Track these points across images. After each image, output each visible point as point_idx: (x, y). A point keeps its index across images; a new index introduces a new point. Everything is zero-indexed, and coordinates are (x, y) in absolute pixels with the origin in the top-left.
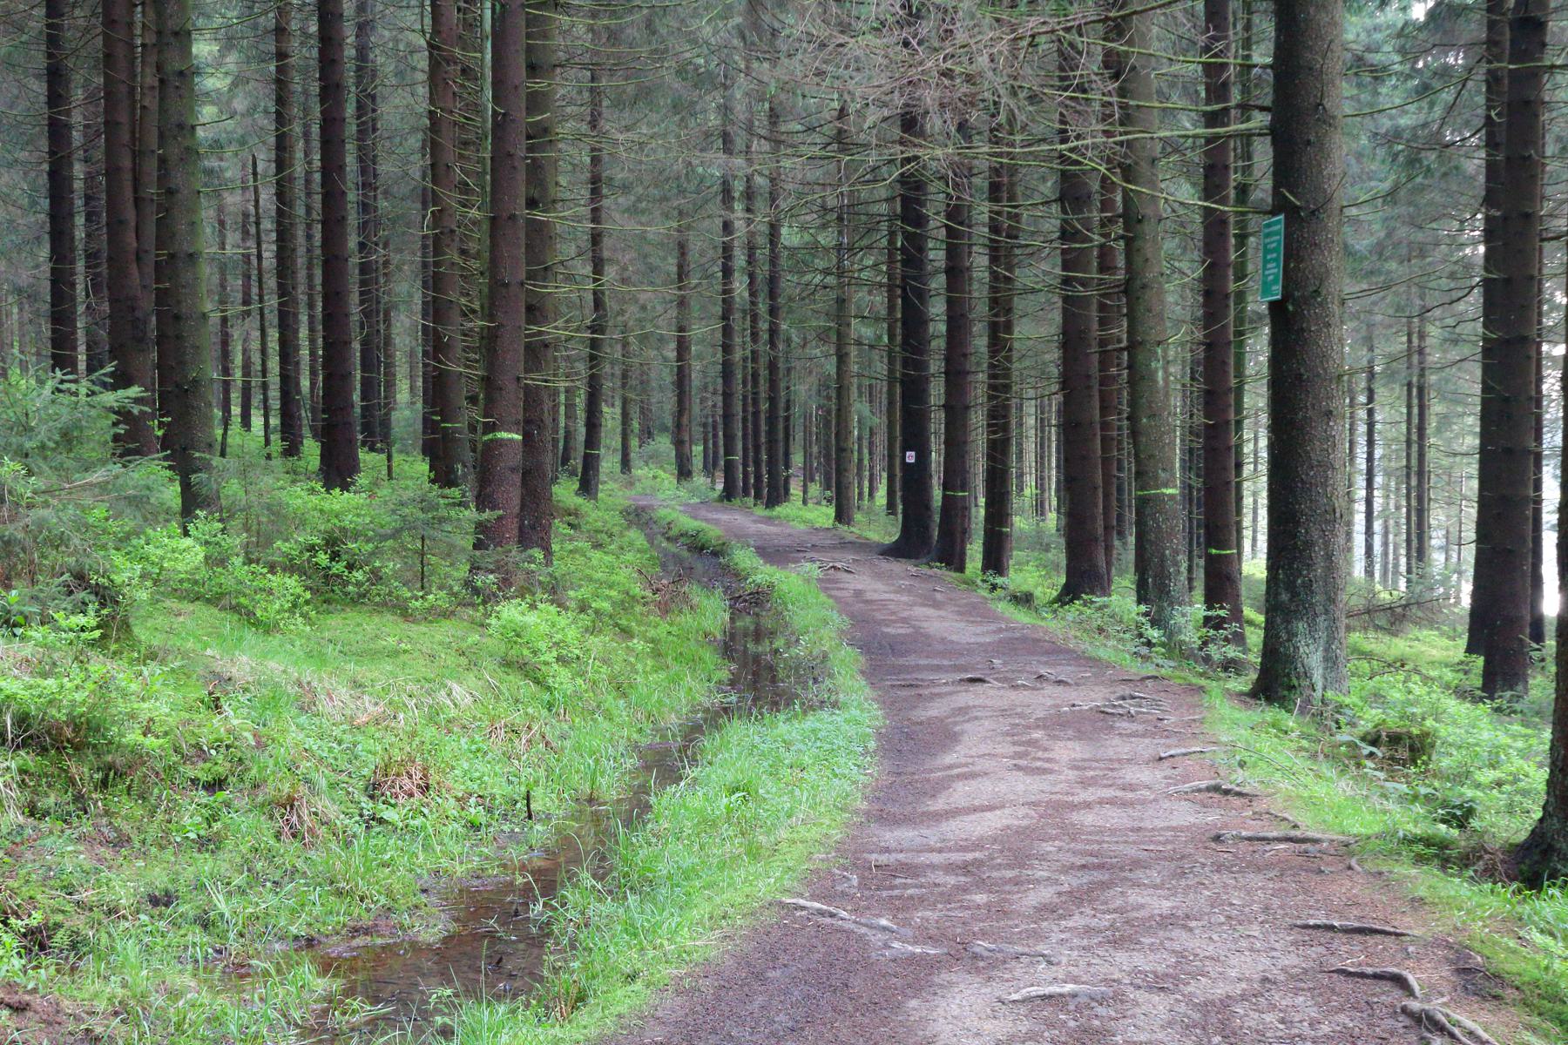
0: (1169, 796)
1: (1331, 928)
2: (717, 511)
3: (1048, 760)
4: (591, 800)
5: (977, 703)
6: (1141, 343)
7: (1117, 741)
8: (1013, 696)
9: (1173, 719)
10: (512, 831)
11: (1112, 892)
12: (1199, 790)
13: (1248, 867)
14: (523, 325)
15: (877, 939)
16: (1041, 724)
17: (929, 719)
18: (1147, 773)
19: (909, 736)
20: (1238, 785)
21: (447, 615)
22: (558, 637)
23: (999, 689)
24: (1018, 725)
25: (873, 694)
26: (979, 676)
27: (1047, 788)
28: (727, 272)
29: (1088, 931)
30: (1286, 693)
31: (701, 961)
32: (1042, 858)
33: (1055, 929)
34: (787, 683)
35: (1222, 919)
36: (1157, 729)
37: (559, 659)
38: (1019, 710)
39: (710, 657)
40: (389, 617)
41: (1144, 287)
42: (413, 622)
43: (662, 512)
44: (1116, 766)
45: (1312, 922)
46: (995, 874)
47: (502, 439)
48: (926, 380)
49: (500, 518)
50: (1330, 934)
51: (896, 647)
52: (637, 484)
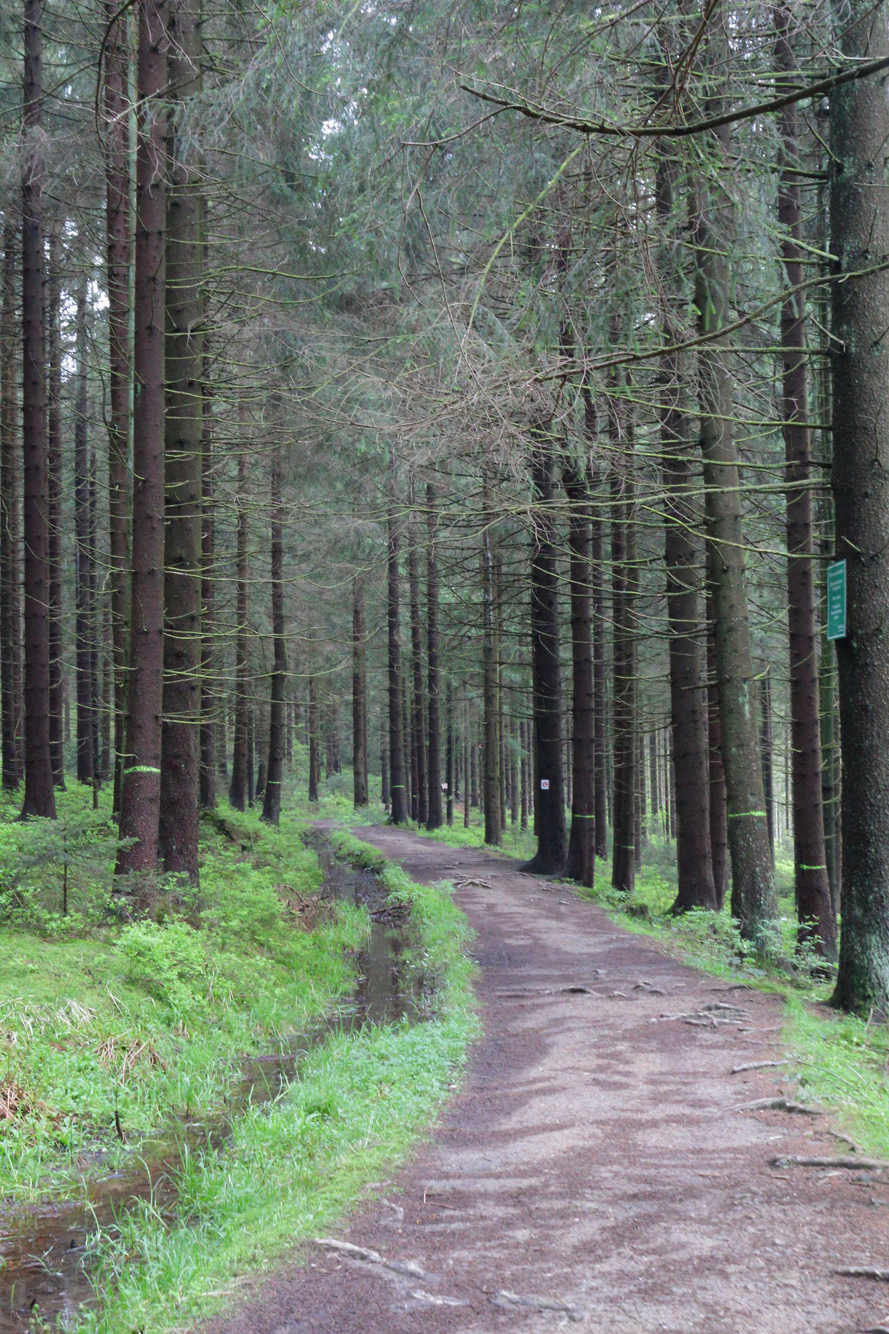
0: (735, 1114)
1: (872, 1276)
2: (384, 832)
3: (627, 1074)
4: (187, 1117)
5: (574, 1014)
6: (729, 681)
7: (696, 1053)
8: (609, 1006)
9: (752, 1029)
10: (100, 1152)
11: (656, 1228)
12: (764, 1108)
13: (799, 1197)
14: (162, 669)
15: (401, 1285)
16: (630, 1036)
17: (525, 1030)
18: (719, 1087)
19: (501, 1049)
20: (803, 1102)
21: (83, 935)
22: (181, 955)
23: (597, 999)
24: (606, 1036)
25: (475, 1003)
26: (580, 987)
27: (619, 1104)
28: (393, 626)
29: (623, 1276)
30: (861, 1003)
31: (209, 1316)
32: (595, 1186)
33: (588, 1274)
34: (408, 993)
35: (762, 1263)
36: (737, 1041)
37: (181, 976)
38: (611, 1021)
39: (339, 967)
40: (29, 938)
41: (730, 630)
42: (50, 942)
43: (336, 834)
44: (691, 1080)
45: (852, 1269)
46: (545, 1205)
47: (141, 773)
48: (558, 717)
49: (137, 844)
50: (871, 1284)
51: (514, 958)
52: (322, 810)
